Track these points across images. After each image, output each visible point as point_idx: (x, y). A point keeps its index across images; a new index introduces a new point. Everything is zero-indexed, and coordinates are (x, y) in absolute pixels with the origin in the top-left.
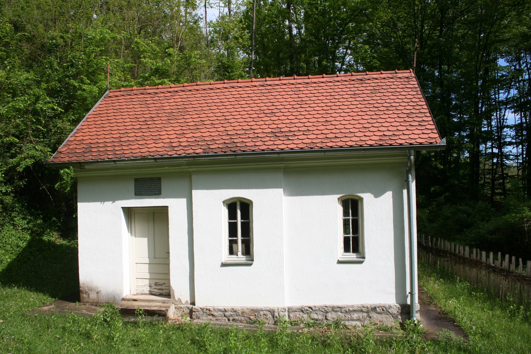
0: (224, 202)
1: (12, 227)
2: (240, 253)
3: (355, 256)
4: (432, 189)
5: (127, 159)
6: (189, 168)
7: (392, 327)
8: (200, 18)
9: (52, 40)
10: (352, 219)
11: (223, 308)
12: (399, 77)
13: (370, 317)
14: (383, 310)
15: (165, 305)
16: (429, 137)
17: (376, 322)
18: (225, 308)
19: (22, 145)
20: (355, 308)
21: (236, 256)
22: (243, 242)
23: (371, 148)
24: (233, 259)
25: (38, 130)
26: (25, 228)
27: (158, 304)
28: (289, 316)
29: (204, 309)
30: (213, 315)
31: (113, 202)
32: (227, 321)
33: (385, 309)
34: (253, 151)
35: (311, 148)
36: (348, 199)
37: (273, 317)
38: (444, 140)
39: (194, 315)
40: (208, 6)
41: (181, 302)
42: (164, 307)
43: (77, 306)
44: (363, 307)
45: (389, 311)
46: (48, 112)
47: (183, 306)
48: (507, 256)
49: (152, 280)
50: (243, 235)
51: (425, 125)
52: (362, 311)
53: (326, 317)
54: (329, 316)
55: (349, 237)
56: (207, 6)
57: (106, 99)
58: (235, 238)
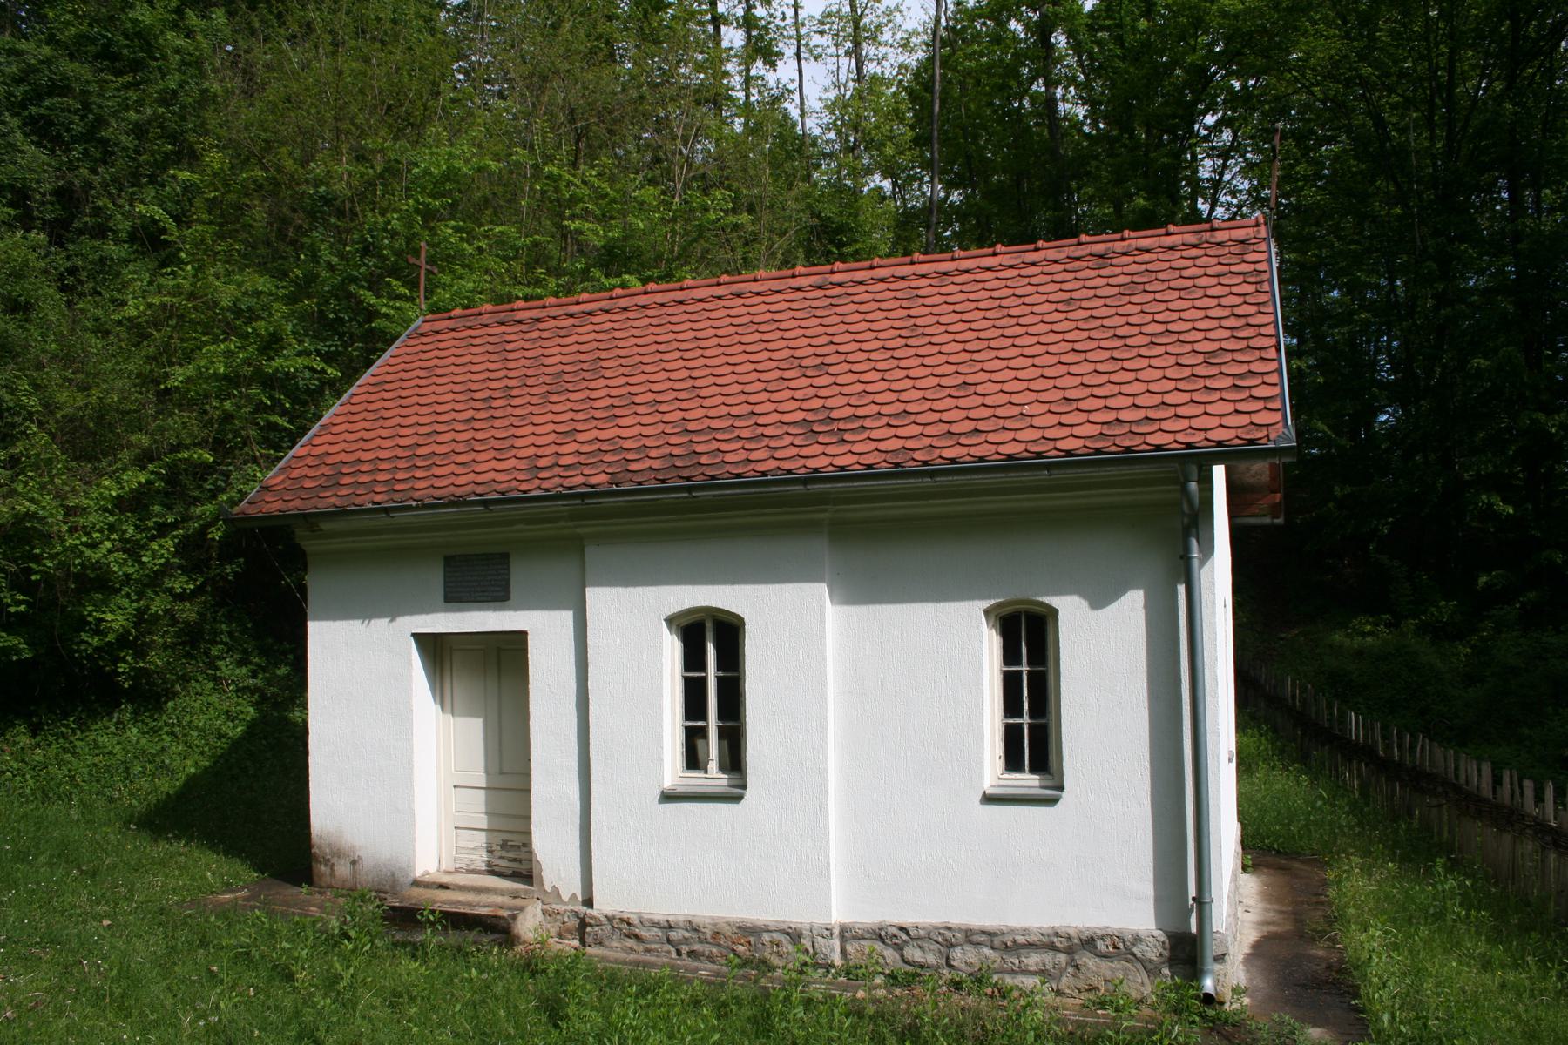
0: (670, 621)
1: (211, 685)
2: (713, 766)
3: (1037, 783)
4: (1483, 579)
5: (414, 504)
6: (576, 527)
7: (1141, 1001)
8: (787, 90)
9: (316, 187)
10: (1029, 673)
11: (666, 918)
12: (1218, 240)
13: (1077, 967)
14: (1116, 947)
15: (518, 902)
16: (1252, 423)
17: (1095, 983)
18: (670, 919)
19: (231, 468)
20: (1032, 938)
21: (702, 775)
22: (722, 733)
23: (1070, 461)
24: (696, 780)
25: (273, 427)
26: (244, 688)
27: (499, 899)
28: (843, 951)
29: (614, 917)
30: (637, 937)
31: (391, 621)
32: (674, 955)
33: (1121, 945)
34: (738, 476)
35: (897, 465)
39: (589, 934)
40: (807, 55)
41: (559, 896)
42: (510, 908)
43: (302, 896)
44: (1057, 934)
45: (1135, 950)
46: (303, 379)
47: (564, 908)
49: (495, 834)
50: (721, 716)
51: (1249, 387)
52: (1052, 947)
53: (948, 958)
54: (957, 955)
55: (1020, 726)
56: (802, 55)
57: (412, 342)
58: (700, 723)
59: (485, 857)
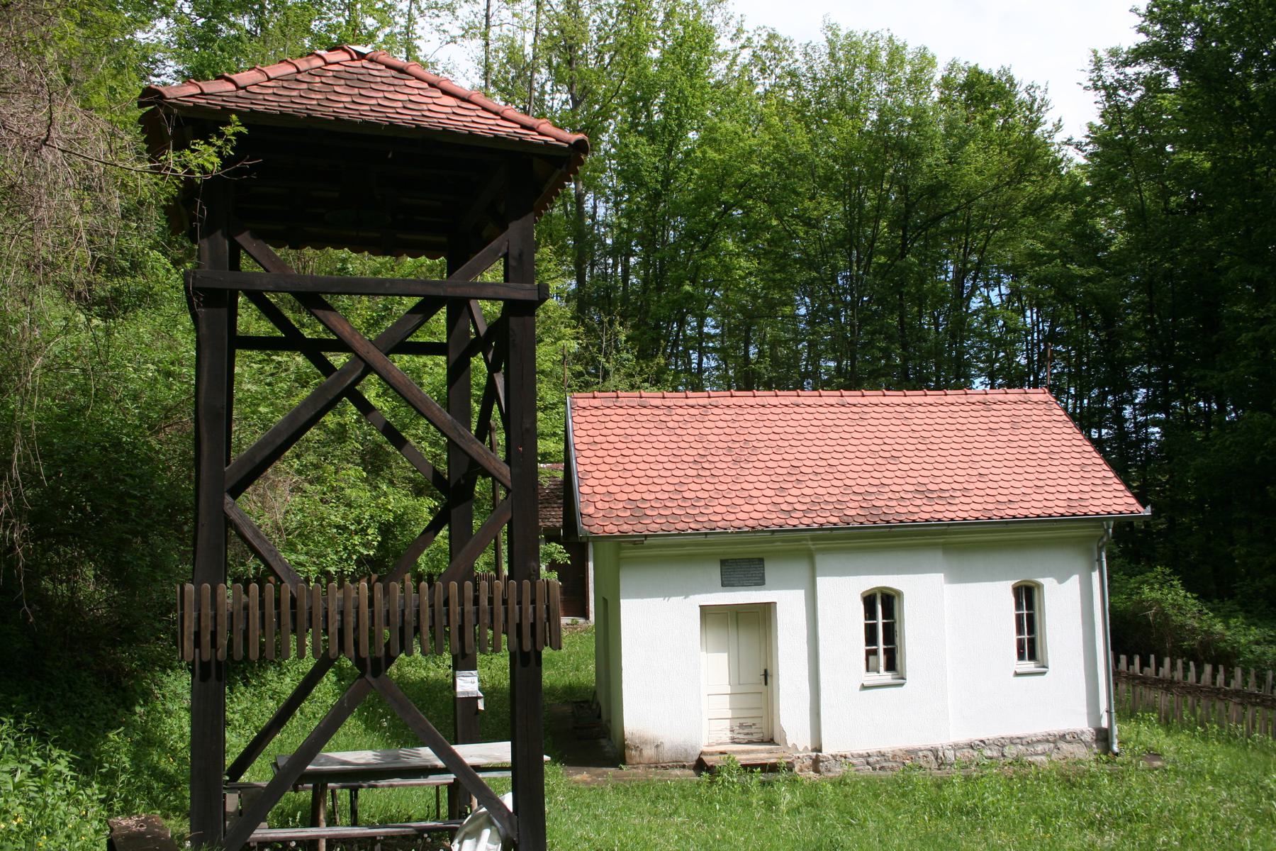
2: (882, 668)
20: (1039, 738)
21: (876, 674)
36: (1021, 587)
37: (937, 759)
38: (1149, 508)
41: (797, 749)
48: (1167, 661)
52: (1048, 741)
54: (1006, 751)
59: (729, 734)
